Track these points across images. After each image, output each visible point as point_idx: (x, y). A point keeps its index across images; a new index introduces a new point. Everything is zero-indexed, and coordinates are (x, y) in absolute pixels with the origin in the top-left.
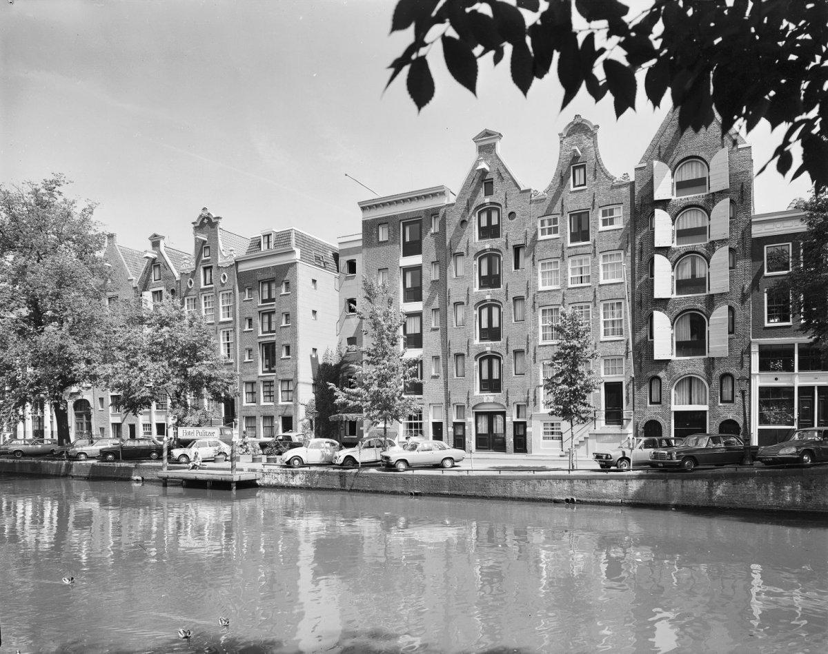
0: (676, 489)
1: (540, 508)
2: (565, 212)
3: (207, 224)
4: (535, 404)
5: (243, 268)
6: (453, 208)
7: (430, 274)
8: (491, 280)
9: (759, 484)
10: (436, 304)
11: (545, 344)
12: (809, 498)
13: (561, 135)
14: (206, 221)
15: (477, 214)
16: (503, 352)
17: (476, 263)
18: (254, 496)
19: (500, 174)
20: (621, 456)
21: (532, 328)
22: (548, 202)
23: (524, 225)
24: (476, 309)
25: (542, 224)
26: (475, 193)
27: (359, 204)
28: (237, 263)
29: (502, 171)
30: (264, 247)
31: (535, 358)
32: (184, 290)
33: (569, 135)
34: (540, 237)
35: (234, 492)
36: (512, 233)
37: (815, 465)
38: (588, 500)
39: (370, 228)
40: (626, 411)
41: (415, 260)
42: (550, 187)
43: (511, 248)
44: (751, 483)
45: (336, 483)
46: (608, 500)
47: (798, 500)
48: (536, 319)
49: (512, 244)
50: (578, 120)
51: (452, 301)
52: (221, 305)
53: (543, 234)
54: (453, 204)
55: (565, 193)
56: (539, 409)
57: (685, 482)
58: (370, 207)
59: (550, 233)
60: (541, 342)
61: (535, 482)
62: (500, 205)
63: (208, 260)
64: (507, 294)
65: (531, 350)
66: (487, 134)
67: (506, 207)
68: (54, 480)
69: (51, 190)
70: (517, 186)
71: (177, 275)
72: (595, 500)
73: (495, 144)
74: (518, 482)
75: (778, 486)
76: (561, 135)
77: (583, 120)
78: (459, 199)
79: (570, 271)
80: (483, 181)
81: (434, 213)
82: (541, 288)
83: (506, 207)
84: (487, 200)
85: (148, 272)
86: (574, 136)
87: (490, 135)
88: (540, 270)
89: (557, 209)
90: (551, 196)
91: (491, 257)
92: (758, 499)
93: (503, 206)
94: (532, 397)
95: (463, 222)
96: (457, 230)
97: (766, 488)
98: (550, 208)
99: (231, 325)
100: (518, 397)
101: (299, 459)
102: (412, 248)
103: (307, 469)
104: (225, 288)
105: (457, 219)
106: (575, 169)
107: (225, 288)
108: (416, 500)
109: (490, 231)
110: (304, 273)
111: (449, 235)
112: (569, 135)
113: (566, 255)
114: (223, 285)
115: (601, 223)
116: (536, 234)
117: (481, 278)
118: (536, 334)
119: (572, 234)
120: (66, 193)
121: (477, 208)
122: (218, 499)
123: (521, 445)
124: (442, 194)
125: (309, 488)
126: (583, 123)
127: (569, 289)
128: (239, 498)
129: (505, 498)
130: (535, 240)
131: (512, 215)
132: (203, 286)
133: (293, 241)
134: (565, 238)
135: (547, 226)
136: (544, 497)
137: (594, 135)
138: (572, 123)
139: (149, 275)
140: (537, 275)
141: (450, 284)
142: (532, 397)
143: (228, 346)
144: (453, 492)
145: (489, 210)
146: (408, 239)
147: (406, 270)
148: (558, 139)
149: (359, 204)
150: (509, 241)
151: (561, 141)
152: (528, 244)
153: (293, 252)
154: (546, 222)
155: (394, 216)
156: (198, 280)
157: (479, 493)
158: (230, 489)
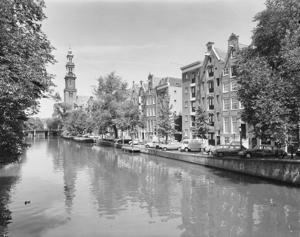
0: (220, 162)
1: (189, 164)
2: (230, 66)
3: (150, 77)
4: (222, 130)
5: (158, 89)
6: (202, 68)
7: (197, 89)
8: (211, 90)
9: (234, 162)
10: (198, 99)
11: (225, 110)
12: (246, 169)
13: (228, 40)
14: (150, 76)
15: (208, 69)
16: (214, 114)
17: (208, 84)
18: (139, 155)
19: (213, 56)
20: (209, 150)
21: (221, 105)
22: (225, 64)
23: (219, 72)
24: (208, 100)
25: (224, 71)
26: (207, 62)
27: (181, 68)
28: (156, 88)
29: (214, 54)
30: (162, 83)
31: (222, 115)
32: (146, 96)
33: (230, 40)
34: (224, 75)
35: (133, 153)
36: (217, 75)
37: (251, 158)
38: (198, 163)
39: (184, 75)
40: (247, 134)
41: (194, 85)
42: (226, 59)
43: (216, 79)
44: (232, 162)
45: (153, 153)
46: (202, 164)
47: (243, 169)
48: (222, 103)
49: (216, 78)
50: (233, 35)
51: (202, 97)
52: (153, 100)
53: (224, 74)
54: (202, 67)
55: (230, 60)
56: (223, 132)
57: (218, 160)
58: (183, 69)
59: (226, 74)
60: (224, 110)
61: (187, 156)
62: (213, 65)
63: (151, 87)
64: (215, 95)
65: (221, 113)
66: (210, 43)
67: (215, 66)
68: (27, 153)
69: (113, 75)
70: (217, 59)
71: (145, 91)
72: (199, 163)
73: (212, 46)
74: (185, 156)
75: (239, 164)
76: (228, 40)
77: (234, 35)
78: (203, 64)
79: (231, 86)
80: (209, 58)
81: (198, 69)
82: (224, 92)
83: (215, 66)
84: (210, 64)
85: (140, 91)
86: (232, 41)
87: (211, 43)
88: (223, 86)
89: (227, 66)
90: (226, 61)
91: (211, 82)
92: (234, 168)
93: (214, 66)
94: (221, 129)
95: (204, 72)
96: (203, 75)
97: (236, 164)
98: (226, 65)
99: (155, 105)
100: (218, 128)
101: (148, 145)
102: (193, 81)
103: (150, 148)
104: (154, 95)
105: (203, 71)
106: (233, 51)
107: (154, 95)
108: (166, 159)
109: (211, 74)
110: (171, 90)
111: (201, 77)
112: (230, 40)
113: (230, 81)
114: (153, 94)
115: (223, 74)
116: (222, 74)
117: (209, 89)
118: (222, 107)
119: (232, 74)
120: (116, 75)
121: (208, 67)
122: (137, 155)
123: (219, 143)
124: (200, 63)
125: (149, 154)
126: (234, 35)
127: (231, 92)
128: (134, 155)
129: (178, 160)
130: (222, 77)
131: (216, 68)
132: (150, 95)
133: (168, 81)
134: (230, 75)
135: (225, 71)
136: (190, 161)
137: (237, 39)
138: (231, 36)
139: (140, 92)
140: (222, 88)
141: (201, 92)
142: (221, 129)
143: (30, 139)
144: (173, 158)
145: (211, 67)
146: (193, 78)
147: (192, 87)
148: (227, 42)
149: (181, 68)
150: (215, 77)
151: (229, 43)
152: (220, 77)
153: (167, 84)
154: (225, 70)
155: (189, 71)
156: (149, 93)
157: (177, 159)
158: (132, 152)
